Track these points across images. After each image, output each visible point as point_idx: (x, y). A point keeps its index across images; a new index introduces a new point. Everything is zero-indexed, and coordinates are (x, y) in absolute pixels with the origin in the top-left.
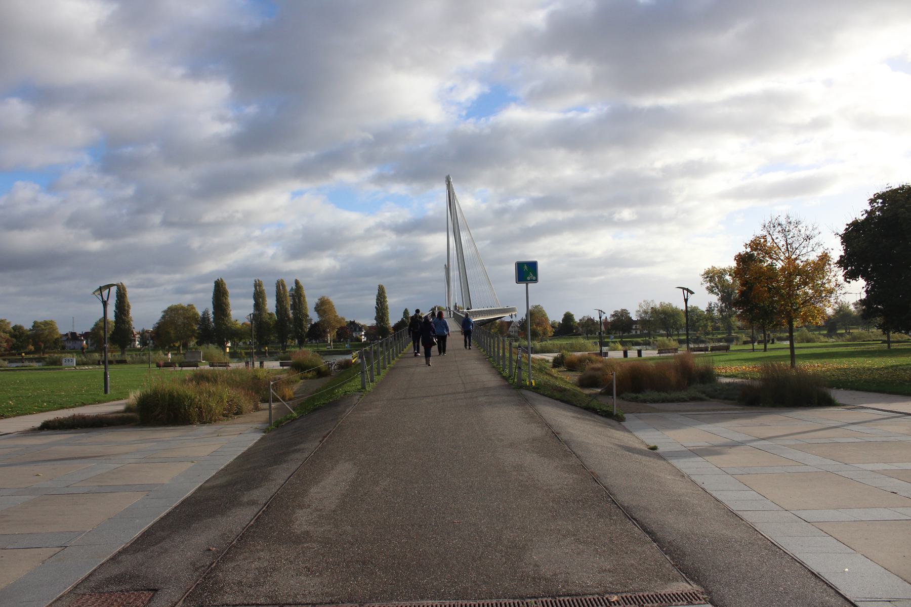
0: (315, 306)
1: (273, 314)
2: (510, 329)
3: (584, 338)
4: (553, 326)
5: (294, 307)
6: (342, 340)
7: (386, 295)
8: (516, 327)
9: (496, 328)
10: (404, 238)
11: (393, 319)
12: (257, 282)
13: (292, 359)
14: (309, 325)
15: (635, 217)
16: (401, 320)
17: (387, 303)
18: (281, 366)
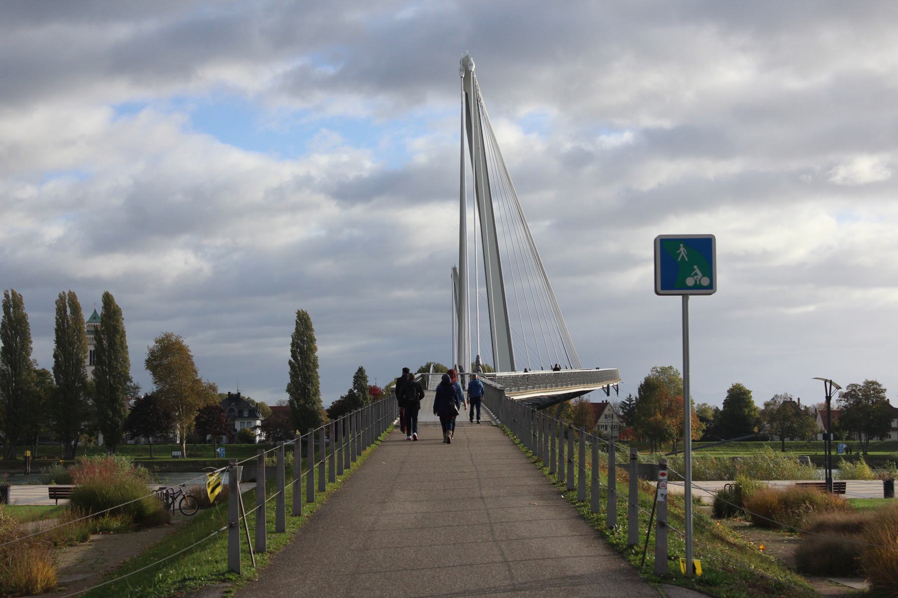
0: (147, 358)
1: (48, 373)
2: (602, 421)
3: (774, 447)
4: (702, 416)
5: (98, 358)
6: (208, 437)
7: (316, 336)
8: (615, 416)
9: (569, 417)
10: (358, 211)
11: (328, 397)
12: (11, 296)
13: (75, 481)
14: (132, 402)
15: (883, 175)
16: (347, 393)
17: (317, 354)
18: (51, 497)
